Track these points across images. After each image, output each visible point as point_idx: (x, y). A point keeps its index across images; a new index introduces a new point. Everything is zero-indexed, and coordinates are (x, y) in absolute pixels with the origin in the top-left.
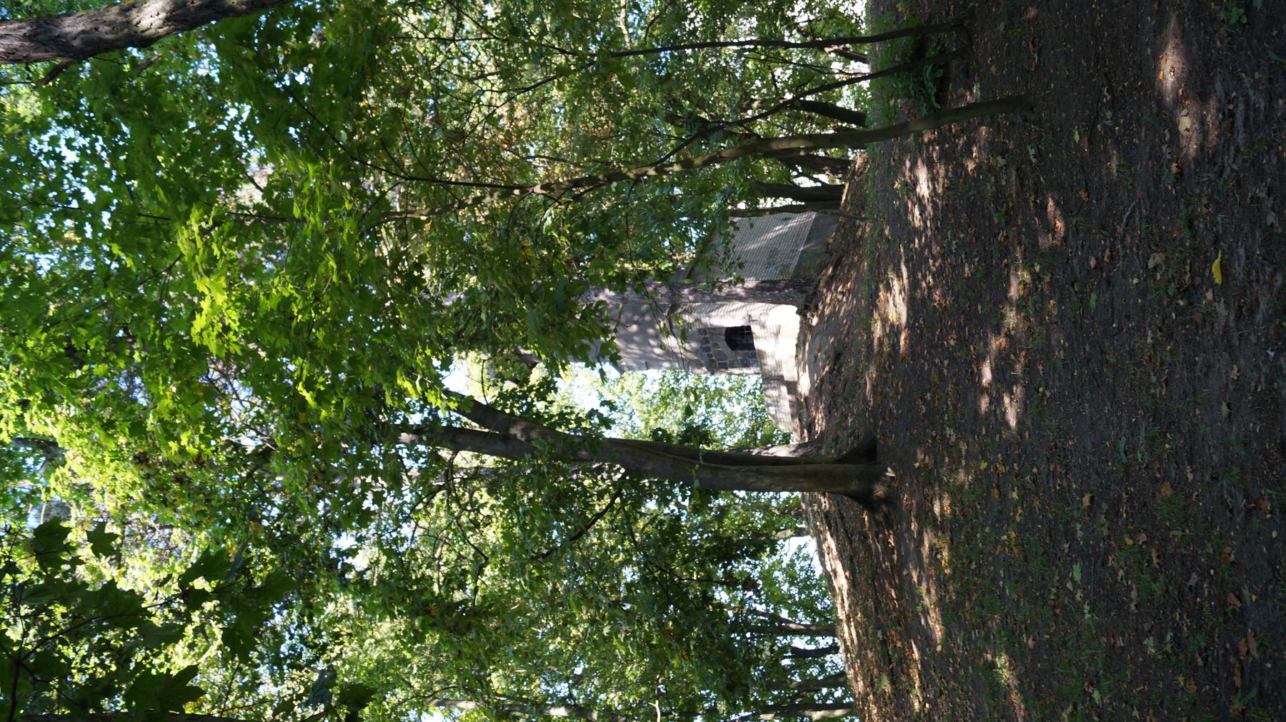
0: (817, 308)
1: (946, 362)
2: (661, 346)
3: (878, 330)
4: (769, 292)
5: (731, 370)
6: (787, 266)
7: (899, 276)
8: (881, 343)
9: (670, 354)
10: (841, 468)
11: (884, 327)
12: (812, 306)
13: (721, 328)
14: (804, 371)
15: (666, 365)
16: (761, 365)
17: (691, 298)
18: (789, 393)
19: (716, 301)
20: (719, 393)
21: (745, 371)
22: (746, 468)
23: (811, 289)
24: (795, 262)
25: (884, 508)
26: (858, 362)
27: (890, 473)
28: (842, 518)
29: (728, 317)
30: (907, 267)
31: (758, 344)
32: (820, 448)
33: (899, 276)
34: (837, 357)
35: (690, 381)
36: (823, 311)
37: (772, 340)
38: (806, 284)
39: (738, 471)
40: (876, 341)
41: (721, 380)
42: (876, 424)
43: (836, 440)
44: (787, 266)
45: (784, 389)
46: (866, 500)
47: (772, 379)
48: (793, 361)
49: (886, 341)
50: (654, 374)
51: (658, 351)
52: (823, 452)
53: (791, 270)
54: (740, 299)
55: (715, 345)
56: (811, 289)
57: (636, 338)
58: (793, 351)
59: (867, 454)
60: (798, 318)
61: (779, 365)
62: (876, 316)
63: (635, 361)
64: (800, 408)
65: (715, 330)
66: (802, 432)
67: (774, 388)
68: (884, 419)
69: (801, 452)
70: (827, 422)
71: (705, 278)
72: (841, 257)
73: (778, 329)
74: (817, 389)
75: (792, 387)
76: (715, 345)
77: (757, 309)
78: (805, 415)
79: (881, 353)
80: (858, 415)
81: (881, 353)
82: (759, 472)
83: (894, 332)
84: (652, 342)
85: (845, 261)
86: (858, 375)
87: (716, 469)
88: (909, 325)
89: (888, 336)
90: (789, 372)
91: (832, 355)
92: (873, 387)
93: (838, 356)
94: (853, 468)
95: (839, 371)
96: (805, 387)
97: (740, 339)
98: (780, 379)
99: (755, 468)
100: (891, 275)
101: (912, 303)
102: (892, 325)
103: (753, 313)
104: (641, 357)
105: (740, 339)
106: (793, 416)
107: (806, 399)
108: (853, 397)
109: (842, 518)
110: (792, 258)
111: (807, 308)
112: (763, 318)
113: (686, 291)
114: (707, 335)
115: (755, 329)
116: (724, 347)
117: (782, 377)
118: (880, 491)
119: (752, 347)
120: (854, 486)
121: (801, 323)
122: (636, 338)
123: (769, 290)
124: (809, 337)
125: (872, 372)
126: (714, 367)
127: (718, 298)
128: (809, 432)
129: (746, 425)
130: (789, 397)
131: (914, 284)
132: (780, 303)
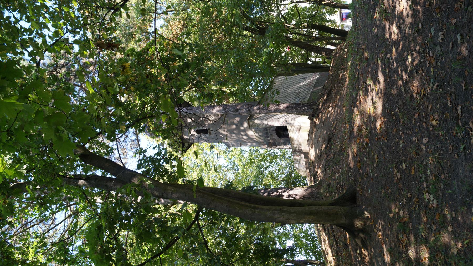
0: (318, 116)
1: (425, 140)
2: (247, 135)
3: (358, 120)
4: (296, 109)
5: (278, 147)
6: (305, 98)
7: (376, 81)
8: (360, 128)
9: (250, 139)
10: (334, 209)
11: (362, 118)
12: (316, 115)
13: (274, 127)
14: (312, 148)
15: (249, 144)
16: (292, 144)
17: (258, 111)
18: (305, 158)
19: (269, 113)
20: (276, 157)
21: (285, 147)
22: (275, 208)
23: (315, 107)
24: (308, 97)
25: (361, 235)
26: (342, 143)
27: (367, 214)
28: (332, 229)
29: (276, 121)
30: (383, 72)
31: (290, 134)
32: (320, 189)
33: (376, 81)
34: (329, 140)
35: (262, 151)
36: (322, 118)
37: (297, 132)
38: (313, 105)
39: (269, 210)
40: (356, 128)
41: (276, 151)
42: (356, 181)
43: (329, 185)
44: (305, 98)
45: (303, 156)
46: (350, 228)
47: (296, 151)
48: (307, 143)
49: (364, 127)
50: (246, 148)
51: (245, 137)
52: (322, 191)
53: (306, 100)
54: (281, 111)
55: (271, 135)
56: (315, 107)
57: (235, 132)
58: (307, 137)
59: (350, 199)
60: (309, 121)
61: (300, 144)
62: (356, 111)
63: (234, 142)
64: (310, 165)
65: (271, 127)
66: (311, 178)
67: (298, 155)
68: (362, 178)
69: (310, 190)
70: (324, 175)
71: (266, 102)
72: (331, 90)
73: (300, 127)
74: (318, 157)
75: (306, 155)
76: (271, 135)
77: (290, 118)
78: (312, 169)
79: (360, 136)
80: (343, 173)
81: (360, 136)
82: (281, 211)
83: (372, 119)
84: (242, 133)
85: (333, 92)
86: (343, 150)
87: (255, 208)
88: (384, 114)
89: (366, 124)
90: (305, 147)
91: (327, 138)
92: (354, 157)
93: (330, 139)
94: (341, 209)
95: (330, 147)
96: (312, 155)
97: (282, 132)
98: (301, 151)
99: (279, 208)
100: (369, 82)
101: (387, 96)
102: (369, 116)
103: (288, 120)
104: (238, 140)
105: (282, 132)
106: (306, 169)
107: (312, 162)
108: (339, 162)
109: (332, 229)
110: (307, 95)
111: (313, 116)
112: (292, 122)
113: (255, 108)
114: (266, 130)
115: (289, 128)
116: (276, 137)
117: (302, 150)
118: (359, 224)
119: (287, 136)
120: (343, 221)
121: (311, 124)
122: (235, 132)
123: (295, 108)
124: (315, 130)
125: (354, 148)
126: (270, 145)
127: (271, 112)
128: (314, 178)
129: (287, 171)
130: (305, 160)
131: (390, 83)
132: (301, 115)
